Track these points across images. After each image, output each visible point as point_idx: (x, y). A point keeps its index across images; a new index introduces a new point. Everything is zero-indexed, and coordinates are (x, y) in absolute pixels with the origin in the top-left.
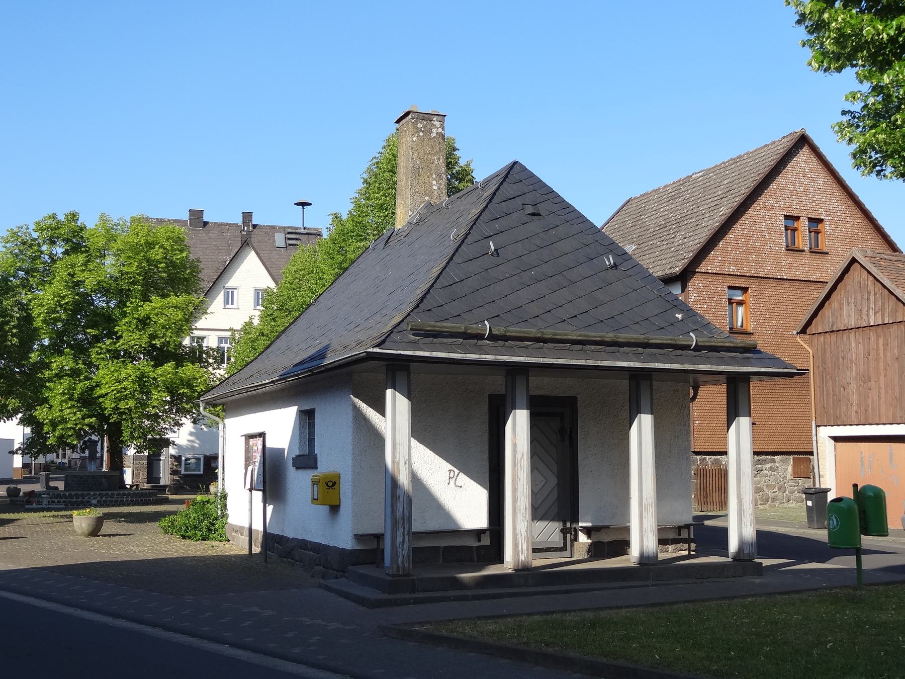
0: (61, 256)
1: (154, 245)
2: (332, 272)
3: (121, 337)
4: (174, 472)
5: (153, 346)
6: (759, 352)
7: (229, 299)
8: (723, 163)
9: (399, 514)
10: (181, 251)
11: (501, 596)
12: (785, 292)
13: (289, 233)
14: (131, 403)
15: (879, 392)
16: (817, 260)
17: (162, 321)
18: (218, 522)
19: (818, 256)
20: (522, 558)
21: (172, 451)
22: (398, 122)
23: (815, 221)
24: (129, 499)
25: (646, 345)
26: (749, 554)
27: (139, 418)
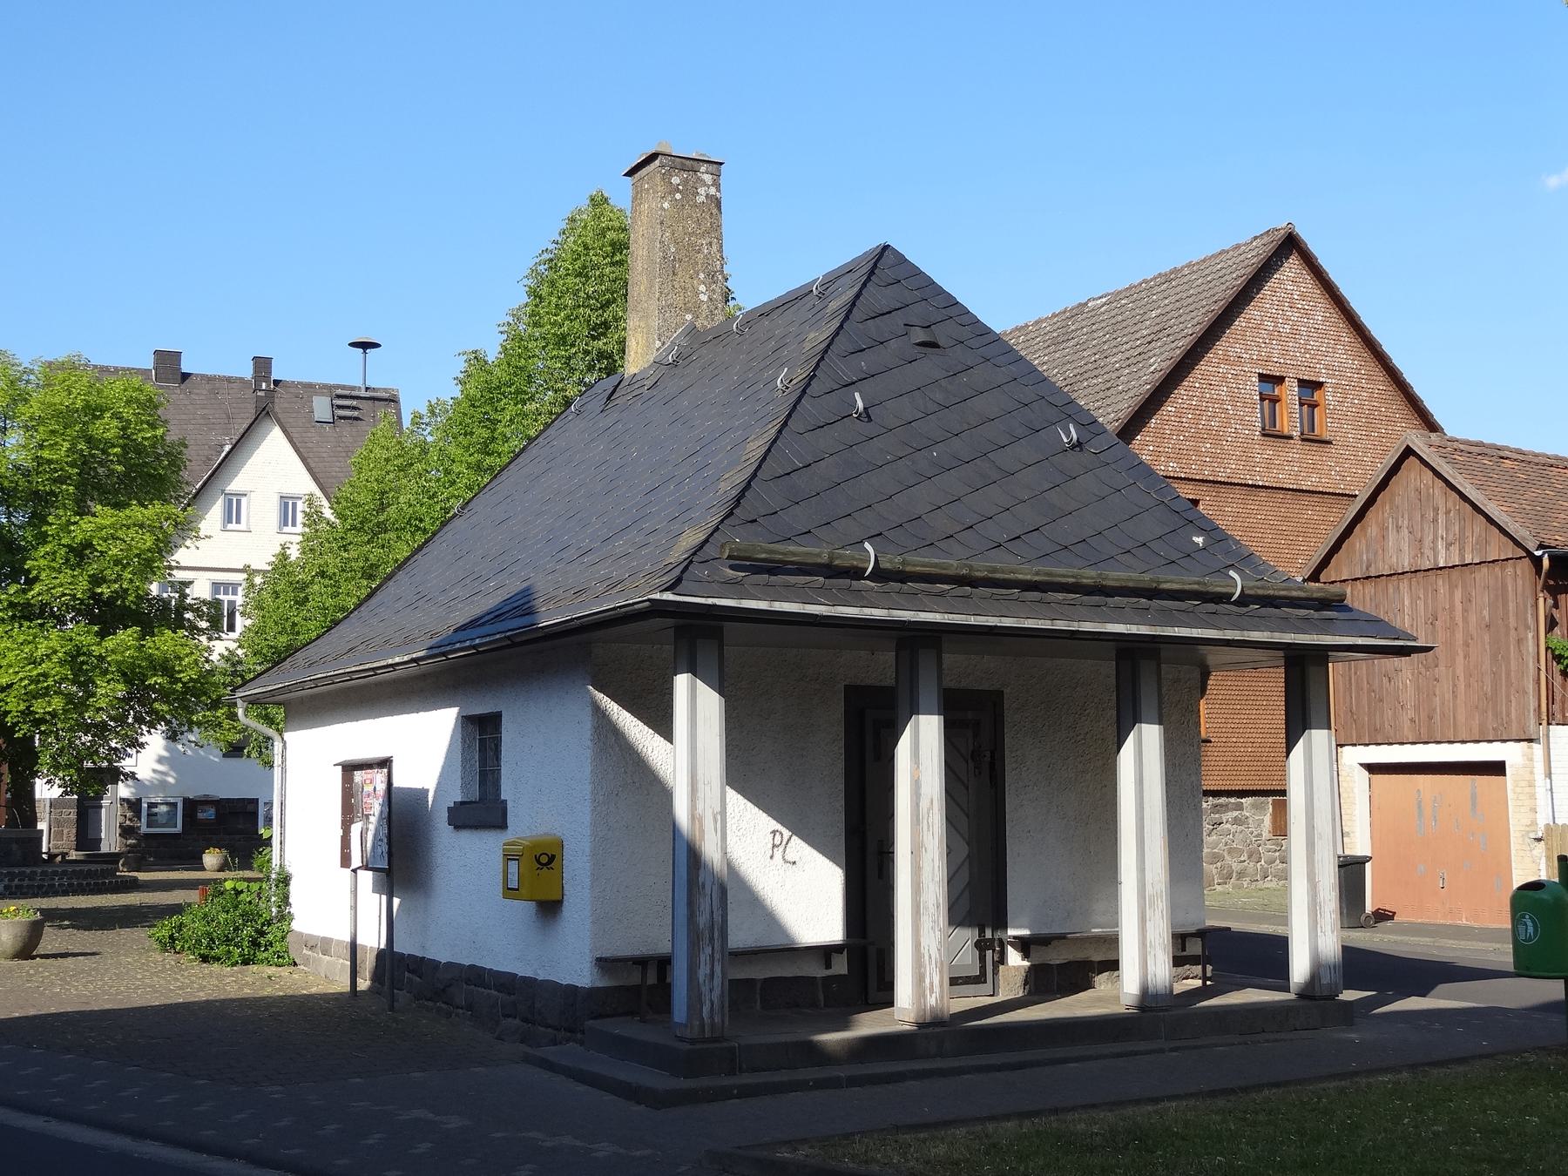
1: (103, 411)
2: (470, 459)
3: (36, 579)
4: (126, 832)
5: (96, 597)
6: (1349, 609)
7: (232, 514)
8: (1145, 281)
9: (703, 920)
10: (153, 426)
13: (339, 397)
14: (57, 703)
15: (1455, 686)
16: (1314, 454)
17: (115, 551)
18: (274, 928)
19: (1315, 447)
20: (932, 1001)
21: (124, 790)
22: (630, 173)
23: (1310, 386)
24: (65, 881)
25: (1153, 593)
27: (71, 729)
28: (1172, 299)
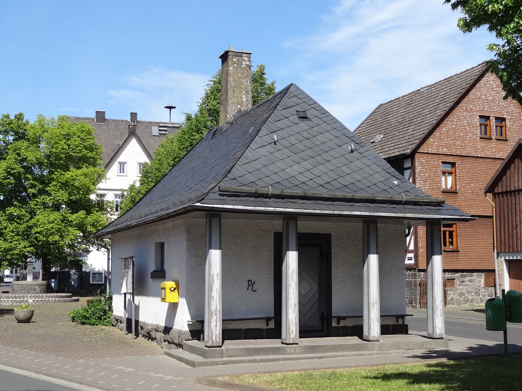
0: (12, 142)
11: (278, 360)
12: (480, 165)
16: (501, 145)
26: (440, 334)
28: (448, 88)
